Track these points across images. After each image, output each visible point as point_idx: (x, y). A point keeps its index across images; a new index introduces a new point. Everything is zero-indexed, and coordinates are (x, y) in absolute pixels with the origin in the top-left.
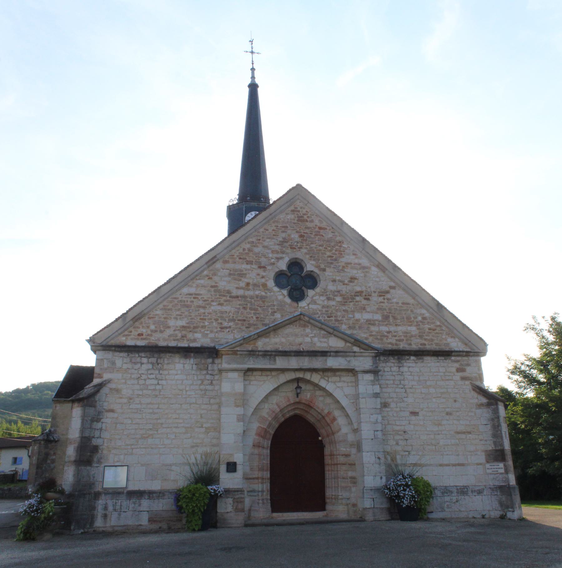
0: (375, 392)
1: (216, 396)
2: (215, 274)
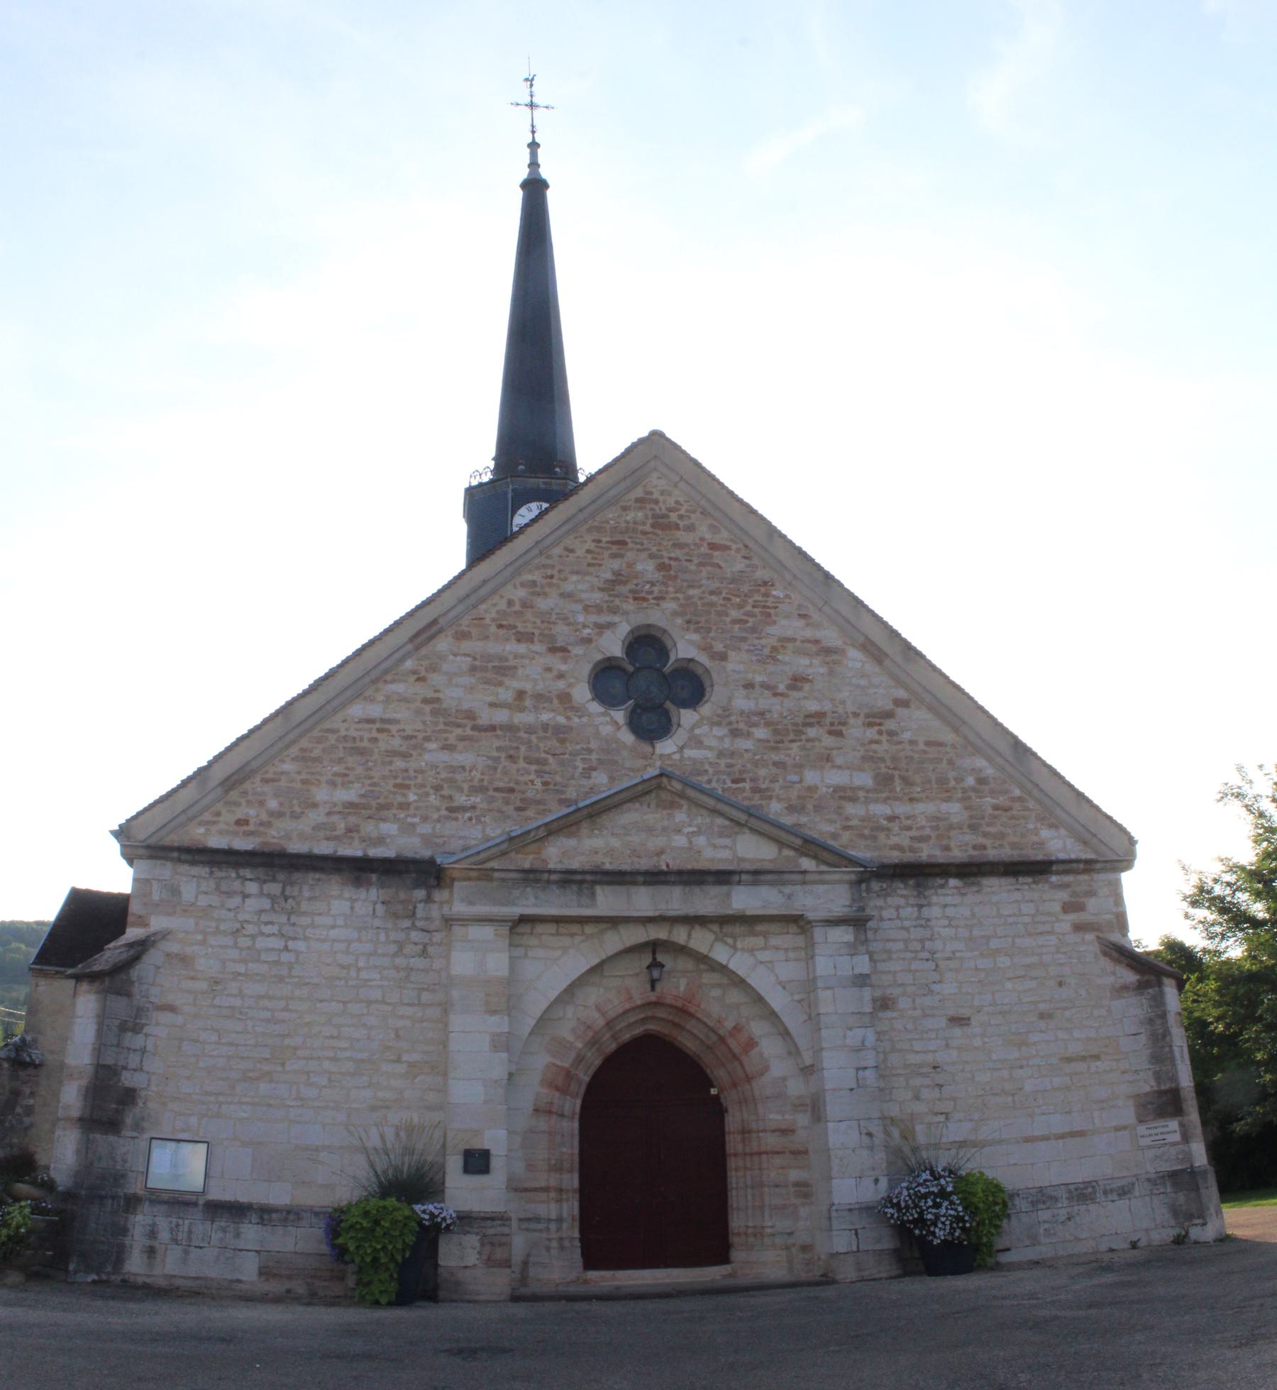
0: (857, 971)
1: (435, 984)
2: (433, 668)
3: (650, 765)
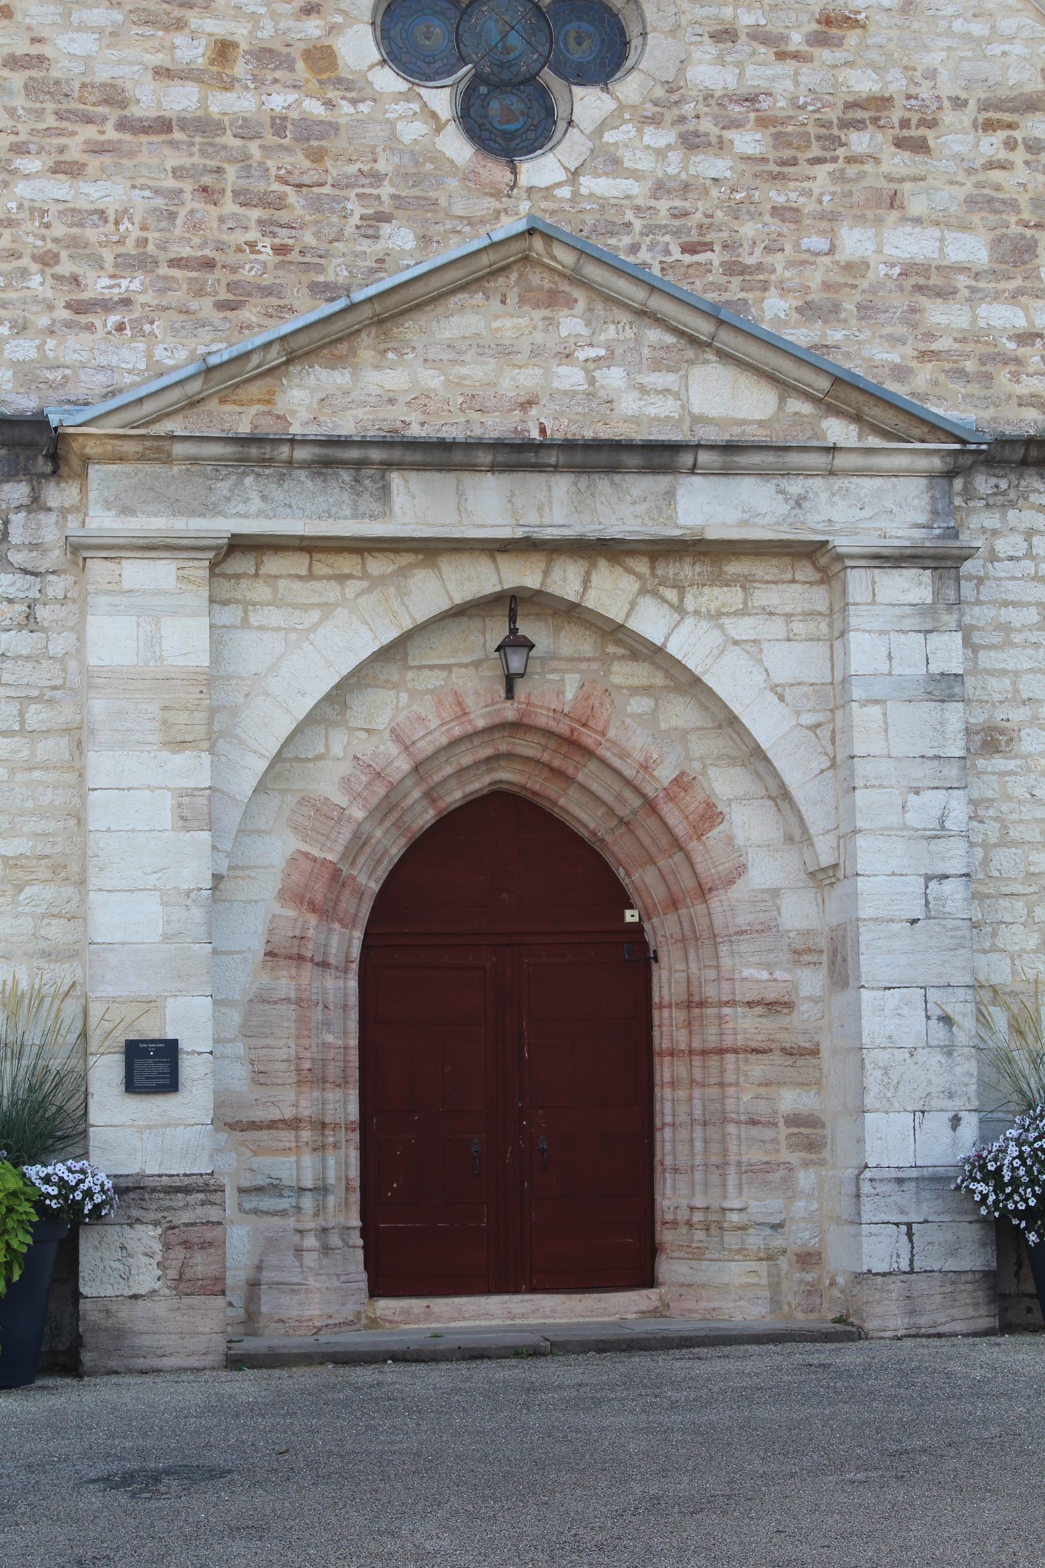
0: (935, 668)
1: (55, 688)
3: (506, 211)
